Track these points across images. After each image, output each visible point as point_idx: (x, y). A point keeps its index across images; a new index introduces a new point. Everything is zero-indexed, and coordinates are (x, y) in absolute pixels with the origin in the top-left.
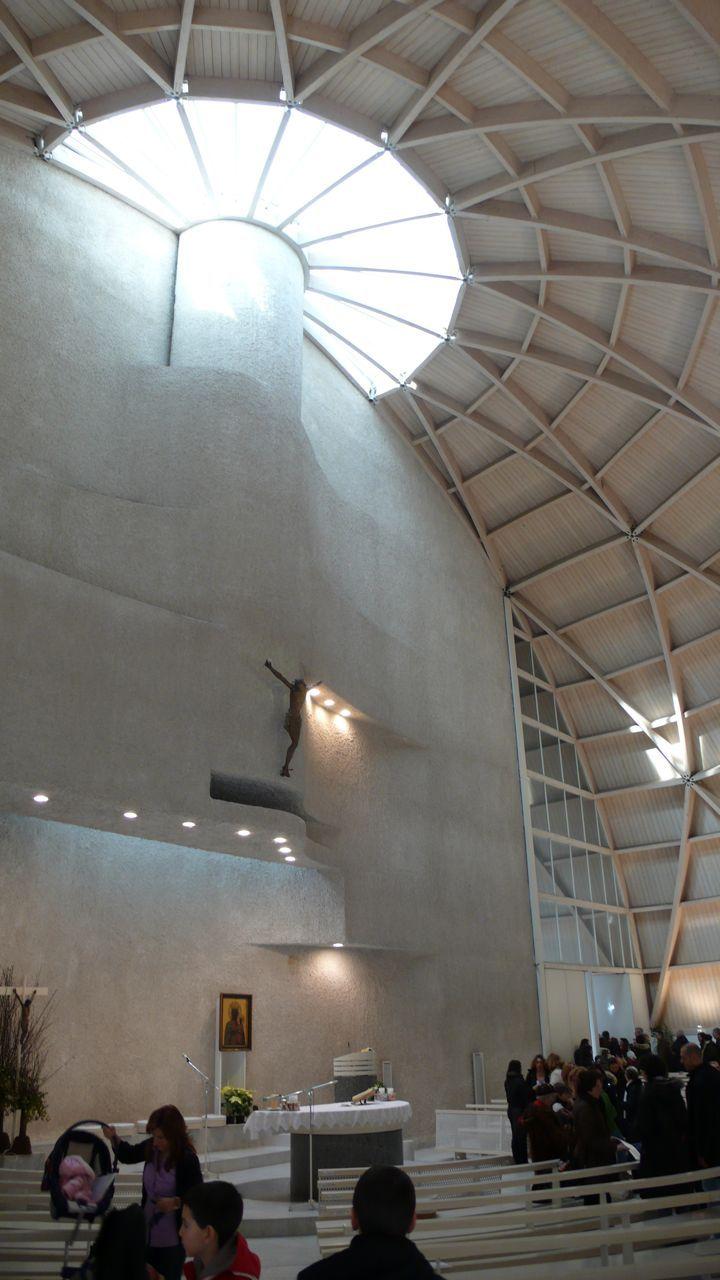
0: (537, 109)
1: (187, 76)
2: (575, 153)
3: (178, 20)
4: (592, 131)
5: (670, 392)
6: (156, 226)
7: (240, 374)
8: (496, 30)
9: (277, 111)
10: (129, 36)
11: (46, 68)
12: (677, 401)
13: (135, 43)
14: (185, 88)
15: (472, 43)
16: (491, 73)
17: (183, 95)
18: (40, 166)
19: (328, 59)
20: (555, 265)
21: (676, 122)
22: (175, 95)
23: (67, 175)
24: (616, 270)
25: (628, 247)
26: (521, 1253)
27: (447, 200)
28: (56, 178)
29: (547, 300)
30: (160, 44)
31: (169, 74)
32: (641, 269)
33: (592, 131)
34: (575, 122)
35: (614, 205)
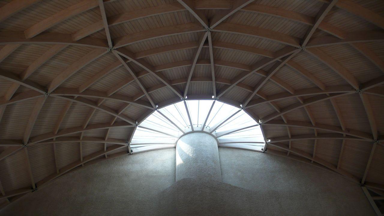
0: (286, 94)
1: (187, 95)
2: (297, 104)
3: (187, 81)
4: (302, 98)
5: (311, 159)
6: (168, 149)
7: (183, 179)
8: (274, 75)
9: (211, 102)
10: (174, 85)
11: (150, 95)
12: (314, 162)
13: (174, 87)
14: (186, 97)
15: (267, 79)
16: (227, 71)
17: (186, 99)
18: (131, 156)
19: (226, 87)
20: (293, 136)
21: (327, 93)
22: (184, 99)
23: (139, 154)
24: (313, 135)
25: (315, 129)
26: (169, 144)
27: (260, 121)
28: (136, 156)
29: (291, 147)
30: (219, 160)
31: (183, 94)
32: (320, 135)
33: (302, 98)
34: (297, 96)
35: (309, 116)
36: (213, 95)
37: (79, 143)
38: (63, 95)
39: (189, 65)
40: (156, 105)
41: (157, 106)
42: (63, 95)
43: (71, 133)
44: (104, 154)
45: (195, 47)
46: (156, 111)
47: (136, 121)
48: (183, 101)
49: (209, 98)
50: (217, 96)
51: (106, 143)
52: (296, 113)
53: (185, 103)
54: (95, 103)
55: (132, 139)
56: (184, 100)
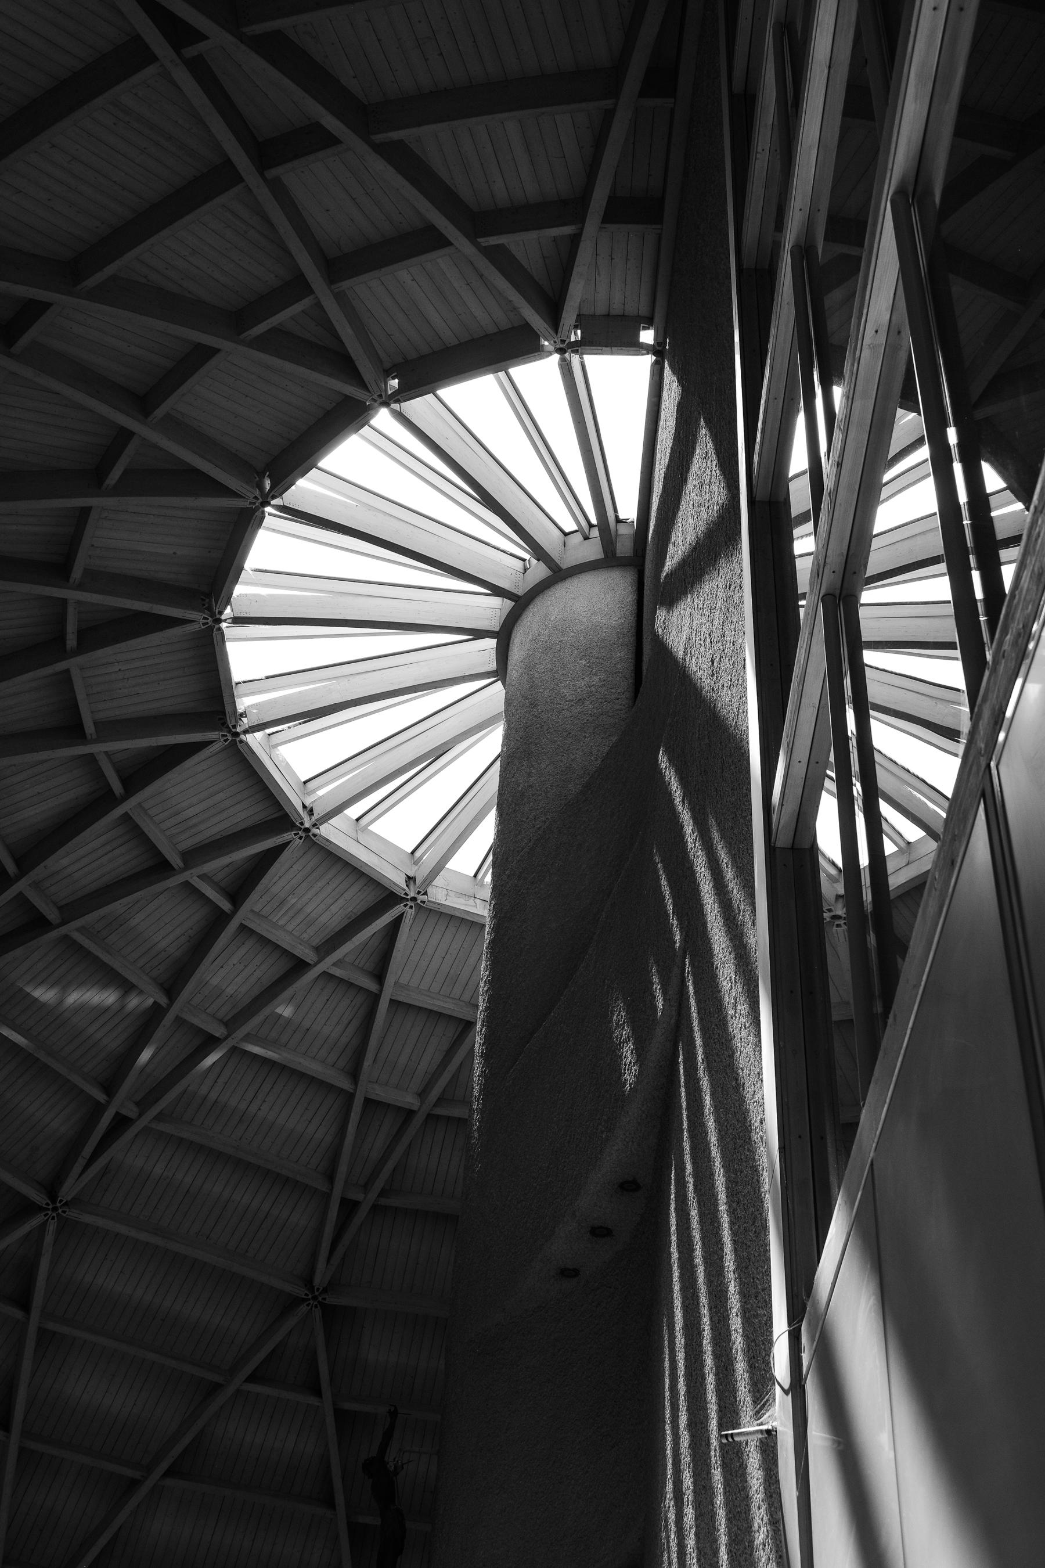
11: (95, 579)
40: (388, 374)
41: (395, 383)
47: (261, 475)
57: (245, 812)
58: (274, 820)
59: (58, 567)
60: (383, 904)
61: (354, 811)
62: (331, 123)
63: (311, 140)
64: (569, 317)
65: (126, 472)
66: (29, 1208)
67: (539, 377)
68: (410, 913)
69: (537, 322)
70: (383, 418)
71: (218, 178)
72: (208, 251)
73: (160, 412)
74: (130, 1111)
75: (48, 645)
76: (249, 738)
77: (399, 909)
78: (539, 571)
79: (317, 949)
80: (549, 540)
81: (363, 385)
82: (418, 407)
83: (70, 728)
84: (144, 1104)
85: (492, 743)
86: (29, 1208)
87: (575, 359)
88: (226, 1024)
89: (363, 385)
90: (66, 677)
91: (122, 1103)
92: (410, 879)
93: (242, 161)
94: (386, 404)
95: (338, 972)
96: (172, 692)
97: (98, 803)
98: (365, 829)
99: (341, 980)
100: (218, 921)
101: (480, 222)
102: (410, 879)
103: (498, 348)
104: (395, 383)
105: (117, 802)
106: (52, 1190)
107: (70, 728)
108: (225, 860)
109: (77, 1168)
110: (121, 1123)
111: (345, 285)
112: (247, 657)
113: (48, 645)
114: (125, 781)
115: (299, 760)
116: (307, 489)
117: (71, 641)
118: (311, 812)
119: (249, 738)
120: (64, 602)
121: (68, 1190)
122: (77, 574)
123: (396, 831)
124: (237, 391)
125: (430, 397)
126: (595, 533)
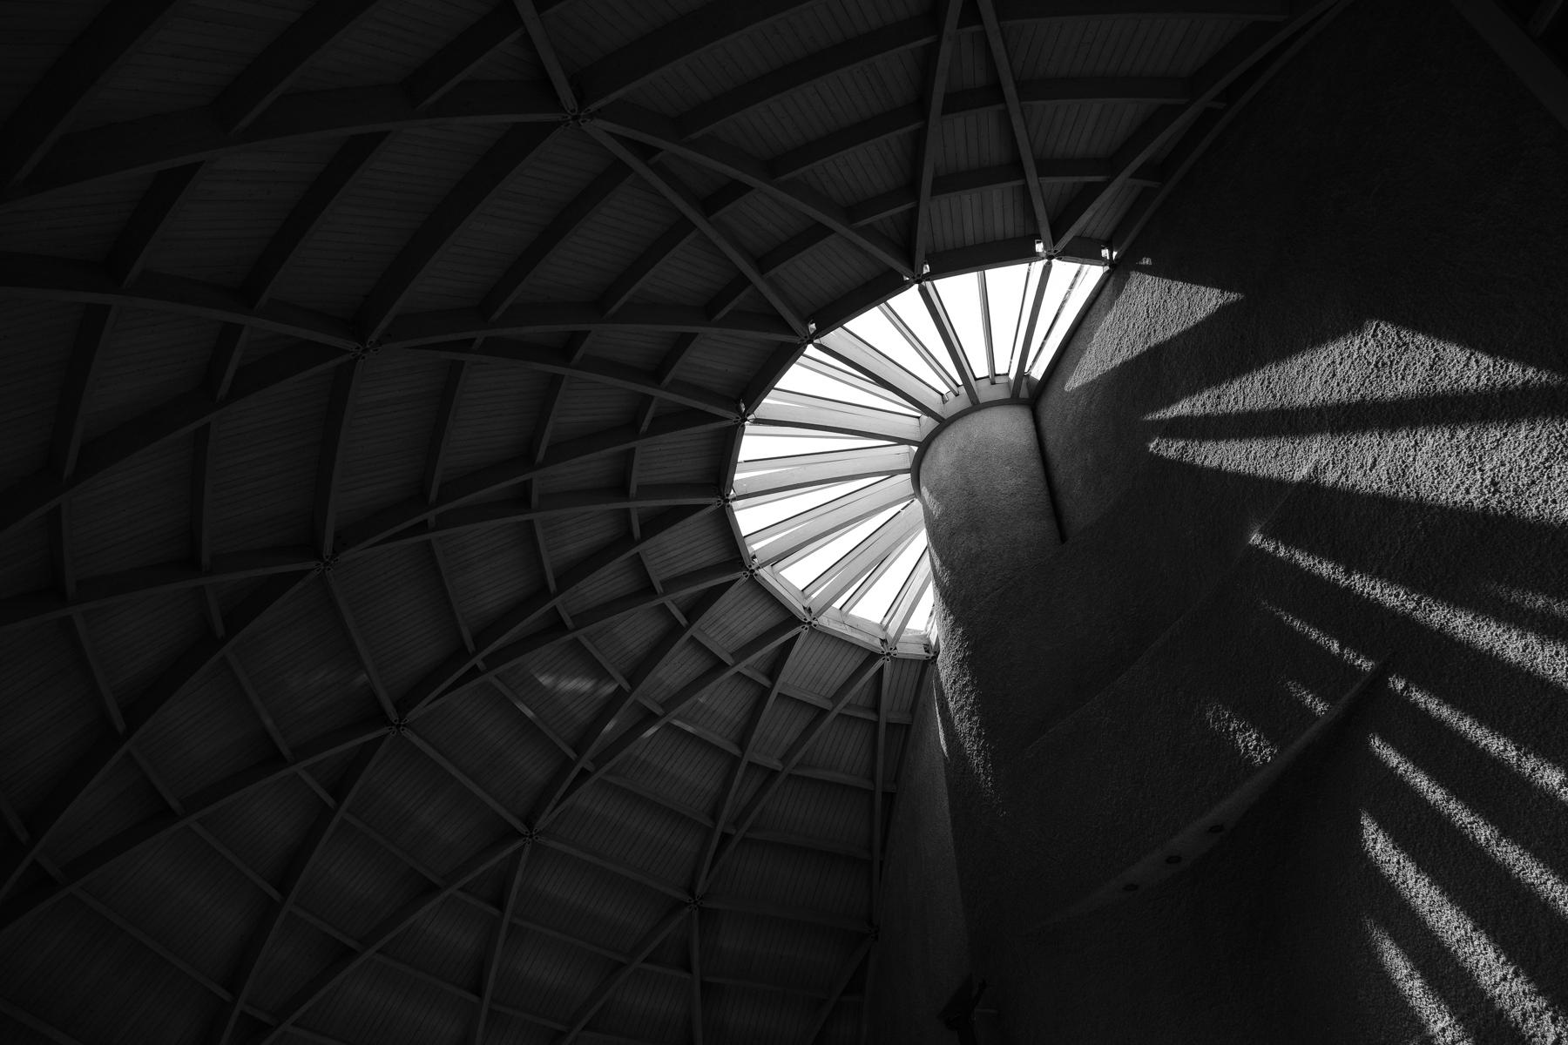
11: (648, 490)
36: (1038, 237)
37: (530, 523)
38: (554, 802)
39: (912, 127)
40: (806, 322)
41: (813, 326)
42: (554, 802)
43: (515, 630)
44: (236, 1012)
45: (926, 41)
46: (810, 346)
47: (737, 402)
48: (916, 286)
49: (1028, 256)
50: (1055, 240)
51: (639, 506)
52: (634, 630)
53: (924, 293)
54: (565, 350)
55: (737, 477)
56: (919, 282)
57: (766, 618)
58: (786, 621)
59: (619, 487)
60: (871, 660)
61: (837, 605)
62: (746, 178)
63: (736, 190)
64: (920, 255)
65: (653, 420)
66: (513, 834)
67: (908, 302)
68: (805, 632)
69: (899, 266)
70: (810, 350)
71: (682, 227)
72: (681, 272)
73: (668, 380)
74: (590, 767)
75: (622, 540)
76: (761, 572)
77: (799, 629)
78: (929, 424)
79: (831, 699)
80: (933, 402)
81: (791, 331)
82: (833, 338)
83: (645, 590)
84: (599, 761)
85: (921, 540)
86: (513, 834)
87: (928, 284)
88: (662, 706)
89: (791, 331)
90: (638, 558)
91: (585, 763)
92: (883, 641)
93: (694, 216)
94: (811, 342)
95: (746, 672)
96: (707, 554)
97: (673, 632)
98: (846, 614)
99: (851, 717)
100: (764, 693)
101: (851, 212)
102: (883, 641)
103: (876, 290)
104: (813, 326)
105: (683, 630)
106: (529, 821)
107: (645, 590)
108: (759, 654)
109: (549, 808)
110: (584, 774)
111: (772, 273)
112: (748, 519)
113: (622, 540)
114: (687, 615)
115: (797, 576)
116: (770, 404)
117: (637, 533)
118: (809, 610)
119: (761, 572)
120: (627, 511)
121: (542, 823)
122: (633, 490)
123: (870, 609)
124: (714, 354)
125: (839, 330)
126: (963, 390)
